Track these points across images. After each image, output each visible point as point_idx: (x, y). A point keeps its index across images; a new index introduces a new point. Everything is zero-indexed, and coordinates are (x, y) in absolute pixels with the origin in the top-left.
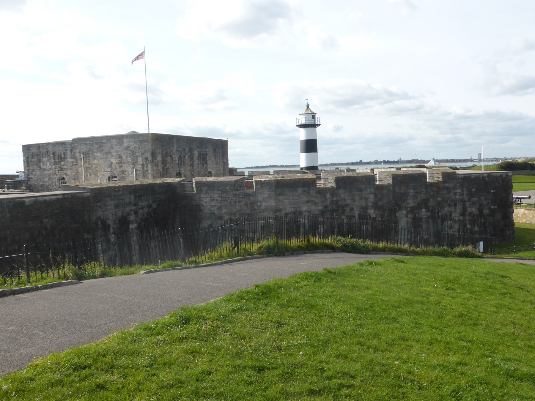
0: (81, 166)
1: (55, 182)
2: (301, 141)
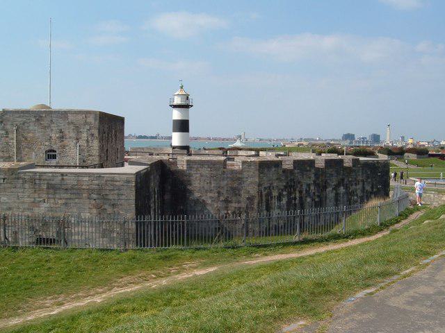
0: (13, 139)
1: (309, 185)
2: (174, 120)
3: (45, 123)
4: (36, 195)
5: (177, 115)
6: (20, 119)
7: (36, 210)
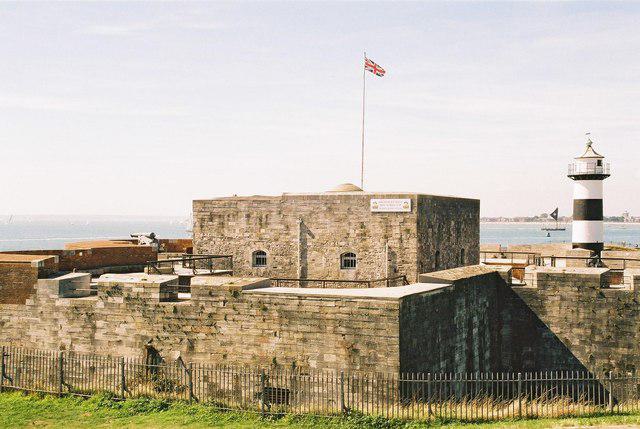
0: (295, 237)
3: (340, 213)
4: (265, 326)
5: (582, 191)
6: (305, 208)
7: (265, 347)
